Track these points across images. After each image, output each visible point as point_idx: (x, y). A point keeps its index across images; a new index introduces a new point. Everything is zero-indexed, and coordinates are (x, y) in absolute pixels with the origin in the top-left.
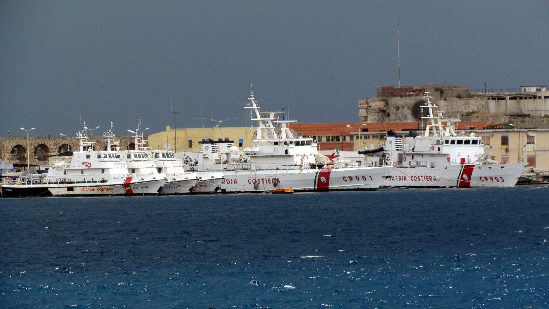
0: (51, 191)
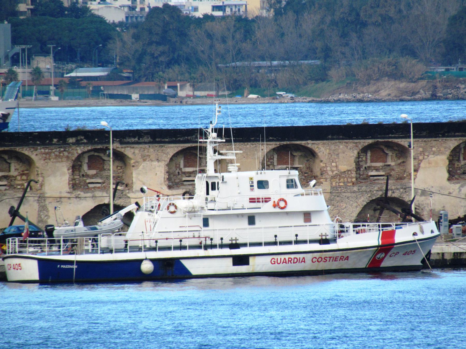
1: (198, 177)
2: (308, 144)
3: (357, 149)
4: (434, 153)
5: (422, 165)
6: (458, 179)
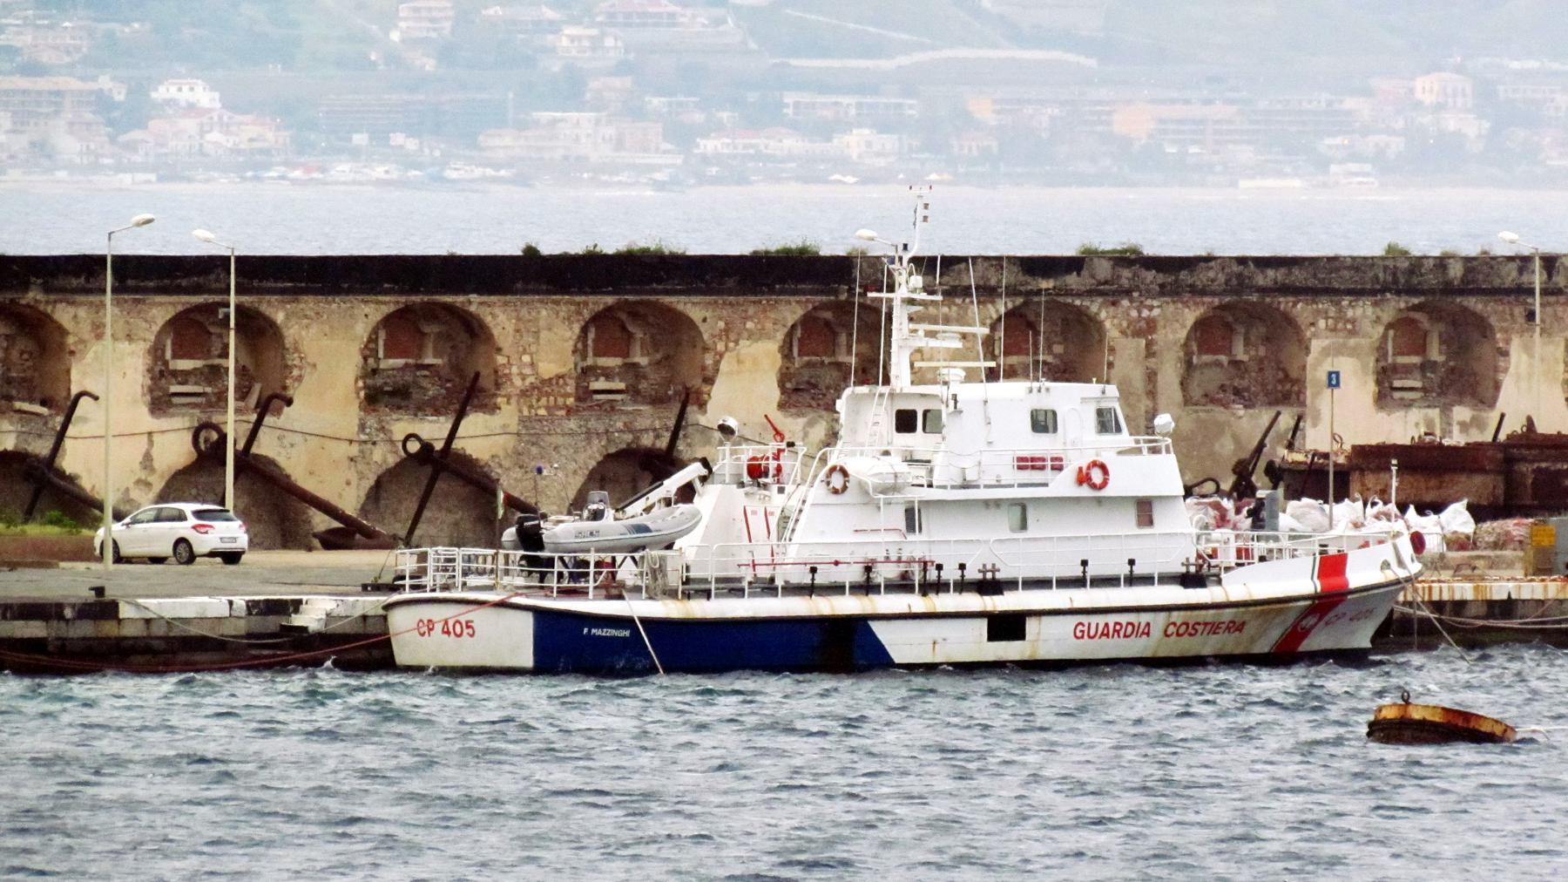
0: (881, 637)
1: (854, 396)
2: (470, 302)
4: (751, 336)
5: (723, 366)
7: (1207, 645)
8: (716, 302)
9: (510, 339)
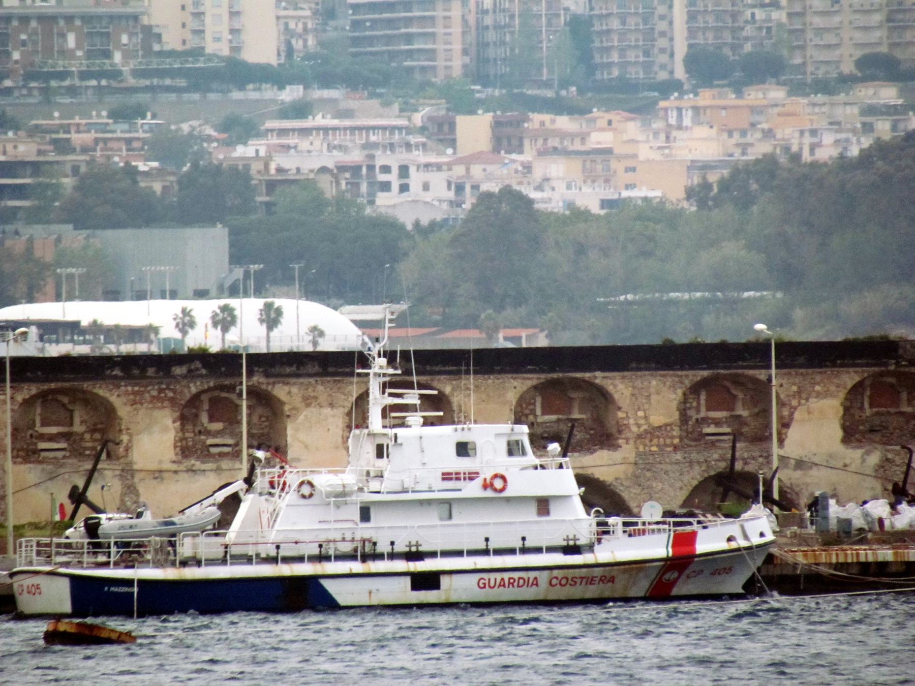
2: (596, 377)
3: (681, 388)
4: (818, 395)
5: (797, 415)
6: (860, 441)
7: (577, 592)
8: (790, 374)
9: (628, 401)
